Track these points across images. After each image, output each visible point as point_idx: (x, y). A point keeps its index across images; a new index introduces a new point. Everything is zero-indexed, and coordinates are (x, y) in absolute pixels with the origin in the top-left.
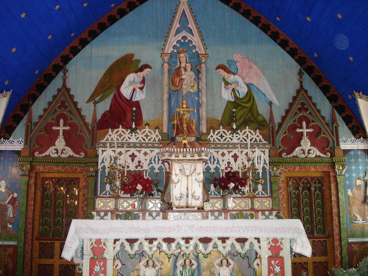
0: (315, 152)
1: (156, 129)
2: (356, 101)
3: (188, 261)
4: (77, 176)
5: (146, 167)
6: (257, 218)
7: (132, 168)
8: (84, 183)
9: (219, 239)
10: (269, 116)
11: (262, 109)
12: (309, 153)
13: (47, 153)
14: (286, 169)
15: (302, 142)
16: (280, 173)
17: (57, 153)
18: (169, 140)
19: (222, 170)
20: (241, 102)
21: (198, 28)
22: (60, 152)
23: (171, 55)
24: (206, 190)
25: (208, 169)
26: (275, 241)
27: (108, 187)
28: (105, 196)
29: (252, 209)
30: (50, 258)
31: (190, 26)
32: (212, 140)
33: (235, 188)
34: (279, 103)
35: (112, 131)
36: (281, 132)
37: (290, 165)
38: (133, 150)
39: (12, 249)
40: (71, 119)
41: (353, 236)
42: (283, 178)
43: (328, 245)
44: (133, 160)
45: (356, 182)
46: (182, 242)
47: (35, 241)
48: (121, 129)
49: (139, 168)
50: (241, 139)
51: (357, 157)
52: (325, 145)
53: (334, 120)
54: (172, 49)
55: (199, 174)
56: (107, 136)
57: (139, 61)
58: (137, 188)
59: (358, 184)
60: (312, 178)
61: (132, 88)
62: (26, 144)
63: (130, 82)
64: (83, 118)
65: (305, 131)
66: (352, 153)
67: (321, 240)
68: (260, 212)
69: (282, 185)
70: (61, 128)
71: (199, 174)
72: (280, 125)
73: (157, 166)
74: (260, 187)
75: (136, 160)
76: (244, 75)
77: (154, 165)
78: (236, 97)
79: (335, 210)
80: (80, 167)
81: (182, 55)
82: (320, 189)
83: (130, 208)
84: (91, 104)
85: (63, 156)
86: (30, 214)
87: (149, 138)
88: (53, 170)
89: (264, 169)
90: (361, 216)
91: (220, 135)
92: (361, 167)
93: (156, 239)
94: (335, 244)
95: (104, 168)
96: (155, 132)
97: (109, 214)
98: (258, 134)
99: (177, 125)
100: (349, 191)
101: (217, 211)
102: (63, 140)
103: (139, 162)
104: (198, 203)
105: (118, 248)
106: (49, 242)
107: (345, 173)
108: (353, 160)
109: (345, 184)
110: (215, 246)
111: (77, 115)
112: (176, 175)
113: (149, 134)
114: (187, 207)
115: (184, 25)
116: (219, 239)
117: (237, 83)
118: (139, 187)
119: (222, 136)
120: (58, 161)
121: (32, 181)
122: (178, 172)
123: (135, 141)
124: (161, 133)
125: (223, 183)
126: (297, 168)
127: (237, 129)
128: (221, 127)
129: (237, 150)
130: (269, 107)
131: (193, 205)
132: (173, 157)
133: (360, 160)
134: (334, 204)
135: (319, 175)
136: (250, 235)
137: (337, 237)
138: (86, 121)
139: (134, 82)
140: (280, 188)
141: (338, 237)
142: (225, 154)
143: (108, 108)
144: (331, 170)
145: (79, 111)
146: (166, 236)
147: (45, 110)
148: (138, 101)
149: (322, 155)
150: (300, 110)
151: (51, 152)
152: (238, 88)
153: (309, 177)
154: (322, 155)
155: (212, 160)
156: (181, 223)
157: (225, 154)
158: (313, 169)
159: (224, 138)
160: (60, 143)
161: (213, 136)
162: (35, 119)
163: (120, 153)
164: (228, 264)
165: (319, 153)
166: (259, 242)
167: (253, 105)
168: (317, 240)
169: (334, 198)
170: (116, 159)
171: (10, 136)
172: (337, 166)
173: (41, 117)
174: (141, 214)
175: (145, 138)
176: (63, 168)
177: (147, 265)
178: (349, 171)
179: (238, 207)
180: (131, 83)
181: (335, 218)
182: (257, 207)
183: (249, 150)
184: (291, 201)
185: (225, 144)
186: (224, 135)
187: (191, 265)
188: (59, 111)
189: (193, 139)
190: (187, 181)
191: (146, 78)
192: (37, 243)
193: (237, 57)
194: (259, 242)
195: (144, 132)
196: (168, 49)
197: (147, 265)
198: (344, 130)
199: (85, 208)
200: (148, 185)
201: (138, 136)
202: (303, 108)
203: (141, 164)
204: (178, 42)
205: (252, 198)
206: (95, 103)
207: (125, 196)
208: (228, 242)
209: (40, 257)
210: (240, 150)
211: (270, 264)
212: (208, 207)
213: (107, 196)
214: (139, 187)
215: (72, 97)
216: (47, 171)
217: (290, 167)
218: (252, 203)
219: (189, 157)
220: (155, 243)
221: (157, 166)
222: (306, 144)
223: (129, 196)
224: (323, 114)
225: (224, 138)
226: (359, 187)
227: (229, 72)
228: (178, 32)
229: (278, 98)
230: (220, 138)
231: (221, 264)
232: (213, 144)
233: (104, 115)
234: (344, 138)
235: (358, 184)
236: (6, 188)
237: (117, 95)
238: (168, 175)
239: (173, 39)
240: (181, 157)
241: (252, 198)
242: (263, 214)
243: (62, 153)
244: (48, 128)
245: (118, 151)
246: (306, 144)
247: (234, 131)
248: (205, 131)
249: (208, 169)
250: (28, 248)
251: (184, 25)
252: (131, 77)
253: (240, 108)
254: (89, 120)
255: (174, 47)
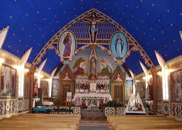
11: (110, 71)
18: (90, 78)
26: (106, 98)
29: (106, 92)
42: (113, 85)
53: (125, 73)
62: (60, 77)
64: (71, 72)
65: (119, 75)
82: (121, 88)
86: (61, 92)
89: (109, 84)
104: (95, 91)
109: (126, 87)
115: (93, 53)
118: (84, 87)
120: (66, 81)
124: (88, 76)
125: (99, 87)
137: (124, 98)
144: (123, 84)
151: (65, 79)
160: (67, 77)
161: (99, 77)
162: (61, 72)
163: (80, 80)
173: (62, 71)
178: (128, 84)
180: (82, 64)
183: (106, 80)
189: (95, 78)
190: (93, 86)
192: (62, 98)
193: (105, 59)
198: (127, 75)
202: (118, 71)
208: (99, 98)
212: (97, 91)
214: (84, 87)
215: (69, 67)
222: (119, 78)
228: (92, 54)
236: (56, 86)
241: (106, 90)
245: (80, 80)
246: (119, 78)
251: (93, 53)
252: (82, 63)
254: (73, 72)
255: (91, 58)
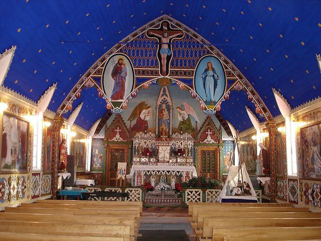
11: (193, 124)
18: (158, 138)
24: (171, 155)
26: (187, 172)
27: (136, 153)
29: (186, 162)
36: (200, 133)
42: (199, 150)
53: (220, 129)
62: (105, 136)
64: (126, 126)
82: (214, 155)
84: (129, 121)
86: (107, 162)
120: (117, 143)
124: (155, 134)
125: (175, 153)
137: (218, 173)
145: (125, 124)
151: (115, 139)
160: (118, 136)
161: (174, 136)
162: (108, 127)
163: (141, 141)
165: (213, 142)
170: (139, 144)
178: (225, 149)
180: (144, 113)
183: (186, 141)
189: (167, 137)
190: (164, 152)
192: (109, 172)
193: (185, 104)
198: (224, 133)
200: (152, 153)
205: (186, 158)
206: (131, 121)
208: (175, 172)
212: (171, 161)
214: (148, 154)
215: (122, 118)
222: (209, 138)
226: (228, 155)
228: (162, 95)
236: (98, 152)
241: (186, 158)
245: (141, 141)
246: (209, 138)
251: (164, 94)
254: (128, 127)
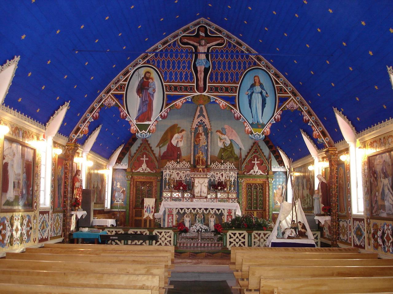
0: (260, 172)
1: (188, 162)
2: (390, 78)
3: (200, 216)
4: (151, 181)
5: (183, 179)
6: (229, 202)
7: (178, 179)
8: (155, 184)
9: (211, 209)
10: (239, 155)
11: (237, 152)
12: (257, 173)
13: (138, 170)
14: (246, 180)
15: (254, 168)
16: (243, 182)
17: (143, 170)
18: (194, 168)
19: (216, 181)
20: (227, 148)
21: (208, 115)
22: (144, 170)
23: (196, 128)
24: (209, 189)
25: (210, 180)
26: (230, 210)
27: (167, 187)
28: (166, 191)
29: (228, 198)
30: (140, 217)
31: (204, 114)
32: (212, 167)
33: (221, 189)
34: (245, 148)
35: (169, 163)
36: (245, 162)
37: (248, 178)
38: (178, 171)
39: (123, 213)
40: (149, 155)
41: (275, 211)
42: (244, 184)
43: (264, 214)
44: (178, 176)
45: (278, 187)
46: (199, 210)
47: (133, 209)
48: (173, 162)
49: (181, 179)
50: (225, 167)
51: (279, 175)
52: (265, 169)
53: (270, 157)
54: (196, 126)
55: (206, 183)
56: (167, 165)
57: (179, 128)
58: (180, 188)
59: (279, 187)
60: (259, 184)
61: (177, 140)
62: (129, 166)
63: (176, 138)
64: (154, 154)
66: (277, 173)
67: (261, 212)
68: (230, 199)
69: (244, 187)
70: (144, 159)
71: (206, 183)
72: (245, 159)
73: (188, 178)
74: (232, 188)
75: (179, 175)
76: (229, 135)
77: (187, 178)
78: (225, 146)
79: (267, 199)
80: (153, 177)
81: (200, 128)
82: (262, 189)
83: (177, 196)
85: (146, 172)
87: (185, 166)
88: (141, 178)
90: (279, 201)
91: (216, 165)
92: (281, 180)
93: (190, 208)
94: (267, 214)
95: (166, 179)
96: (188, 164)
97: (169, 198)
98: (233, 165)
99: (197, 160)
100: (275, 190)
101: (213, 198)
102: (146, 165)
103: (181, 176)
104: (205, 195)
105: (177, 211)
106: (140, 210)
107: (273, 182)
108: (277, 176)
109: (273, 187)
110: (209, 211)
111: (152, 153)
112: (197, 183)
113: (185, 164)
114: (201, 196)
115: (201, 114)
116: (211, 209)
117: (225, 139)
118: (181, 188)
119: (217, 166)
120: (143, 174)
121: (132, 183)
122: (197, 182)
123: (179, 167)
124: (190, 164)
125: (215, 186)
126: (251, 179)
127: (223, 163)
128: (217, 162)
129: (223, 172)
130: (239, 150)
131: (203, 196)
132: (195, 176)
133: (281, 176)
134: (267, 196)
135: (261, 182)
136: (221, 208)
137: (267, 211)
138: (156, 156)
139: (178, 138)
140: (243, 188)
141: (268, 211)
142: (218, 174)
143: (166, 150)
144: (267, 181)
145: (152, 151)
146: (193, 207)
147: (137, 150)
148: (179, 147)
149: (263, 174)
150: (254, 152)
151: (140, 170)
152: (226, 142)
153: (257, 183)
154: (263, 174)
155: (212, 176)
156: (198, 203)
157: (218, 174)
158: (258, 180)
159: (218, 167)
160: (144, 166)
161: (213, 166)
162: (133, 154)
164: (213, 217)
165: (261, 173)
166: (224, 210)
167: (232, 150)
168: (259, 212)
169: (267, 193)
170: (171, 175)
171: (121, 162)
172: (269, 179)
173: (135, 154)
174: (182, 199)
175: (183, 166)
176: (146, 177)
177: (187, 217)
178: (275, 181)
179: (222, 197)
180: (176, 138)
181: (267, 202)
182: (230, 197)
183: (228, 172)
184: (248, 194)
185: (218, 169)
186: (217, 165)
187: (201, 217)
188: (143, 151)
189: (204, 167)
190: (201, 185)
191: (183, 136)
192: (134, 210)
193: (226, 126)
194: (224, 210)
195: (183, 163)
196: (194, 126)
197: (187, 217)
198: (274, 162)
199: (156, 195)
201: (180, 165)
203: (182, 177)
204: (199, 122)
205: (228, 193)
206: (160, 147)
207: (175, 191)
208: (214, 210)
209: (136, 216)
210: (224, 172)
211: (227, 217)
212: (209, 196)
213: (167, 191)
214: (181, 188)
215: (149, 144)
216: (138, 178)
217: (248, 179)
218: (228, 195)
219: (202, 176)
220: (190, 210)
221: (188, 178)
222: (256, 168)
223: (176, 191)
224: (265, 154)
225: (218, 167)
226: (279, 189)
227: (222, 134)
228: (199, 116)
229: (244, 146)
230: (216, 166)
231: (211, 217)
232: (212, 169)
233: (164, 153)
234: (274, 166)
235: (279, 187)
236: (120, 186)
237: (170, 144)
238: (193, 183)
239: (196, 120)
240: (199, 176)
241: (228, 193)
242: (232, 200)
243: (145, 170)
244: (138, 159)
245: (173, 172)
246: (256, 168)
247: (222, 164)
248: (209, 164)
249: (210, 180)
250: (131, 213)
251: (201, 114)
252: (176, 135)
253: (226, 151)
254: (157, 155)
255: (197, 125)
